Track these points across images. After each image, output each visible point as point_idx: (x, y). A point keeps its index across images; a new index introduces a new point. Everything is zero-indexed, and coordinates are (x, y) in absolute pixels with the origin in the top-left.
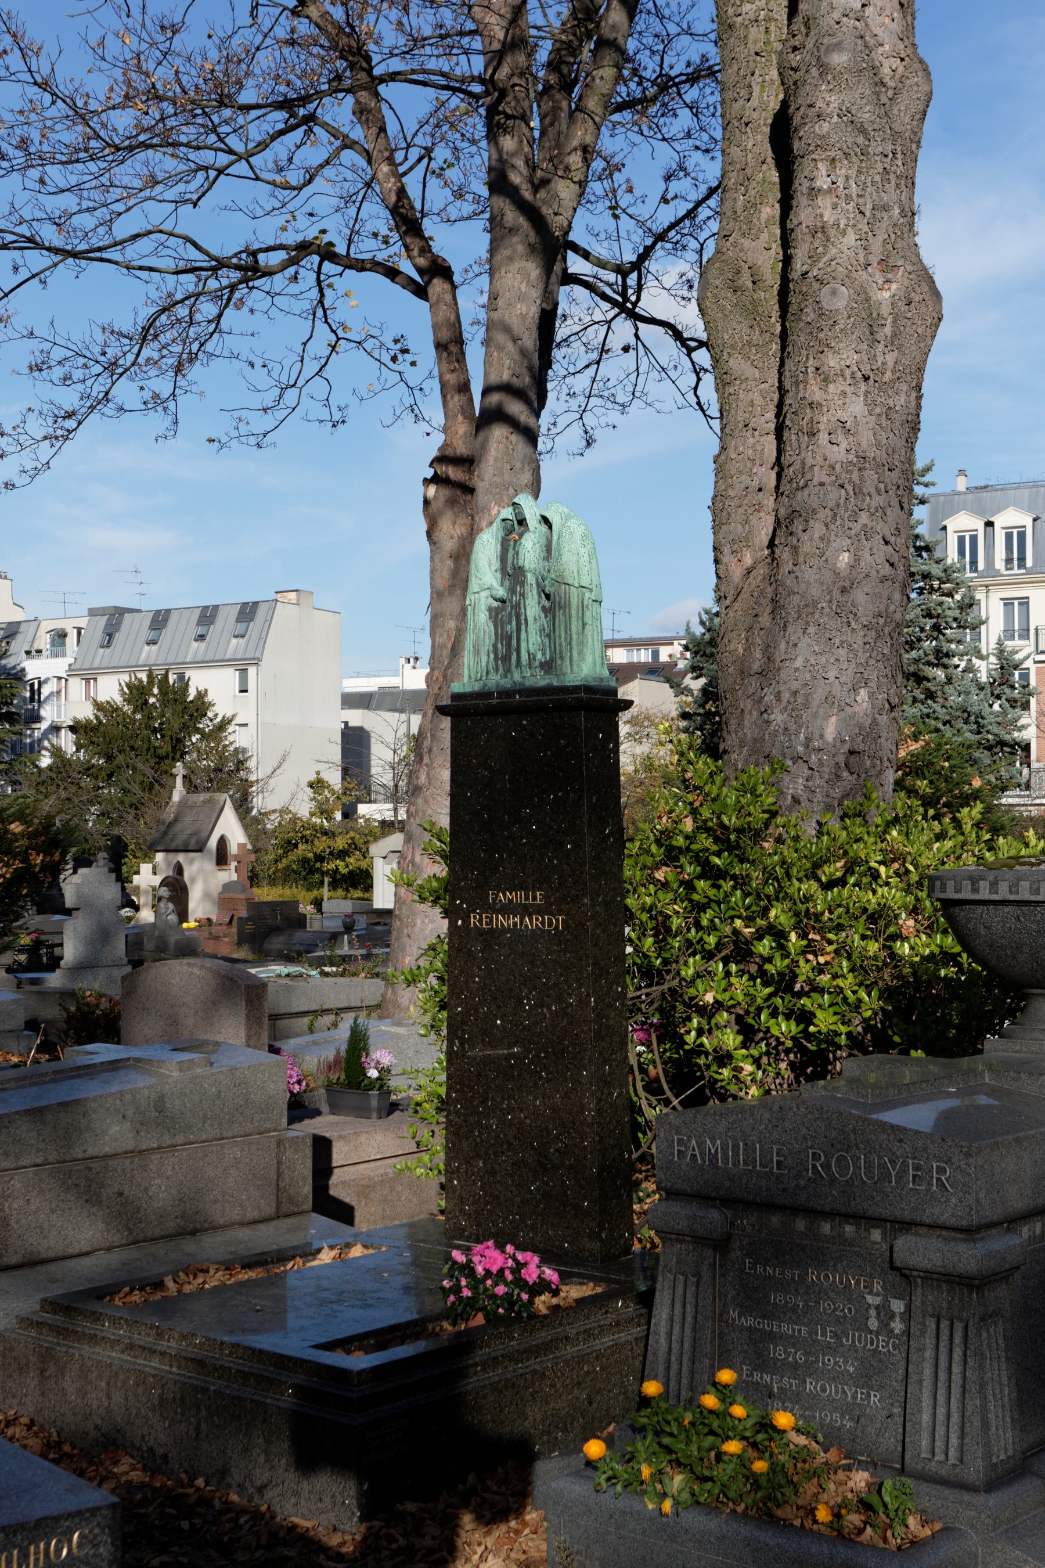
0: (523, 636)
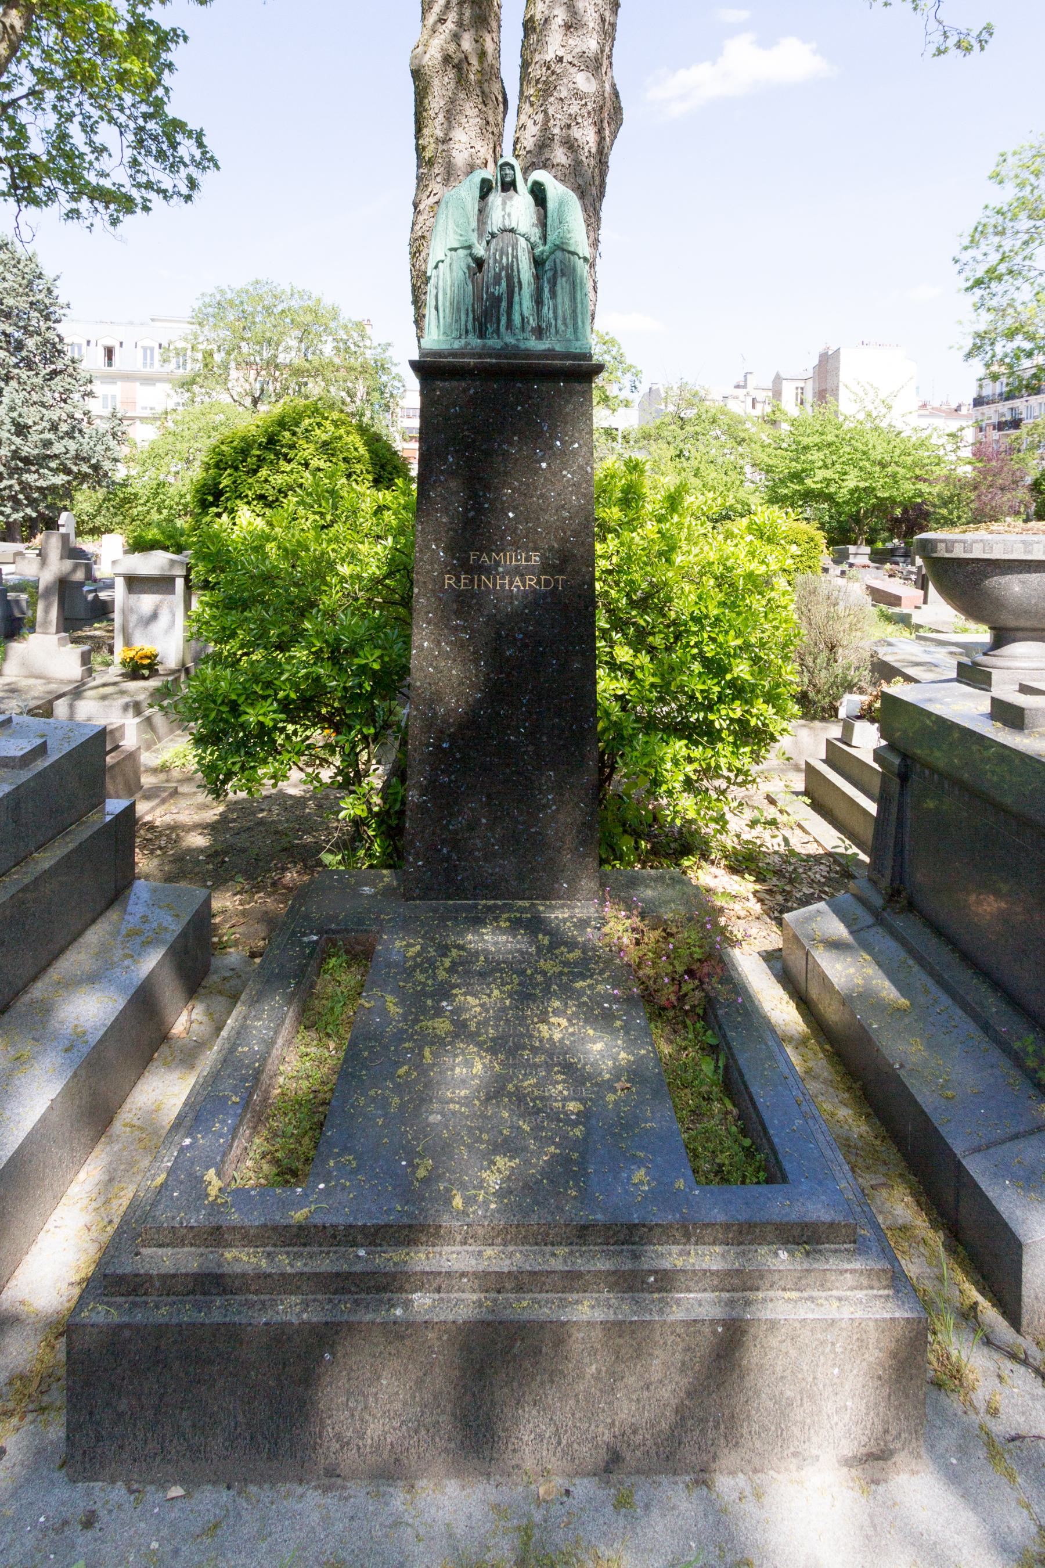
0: (516, 298)
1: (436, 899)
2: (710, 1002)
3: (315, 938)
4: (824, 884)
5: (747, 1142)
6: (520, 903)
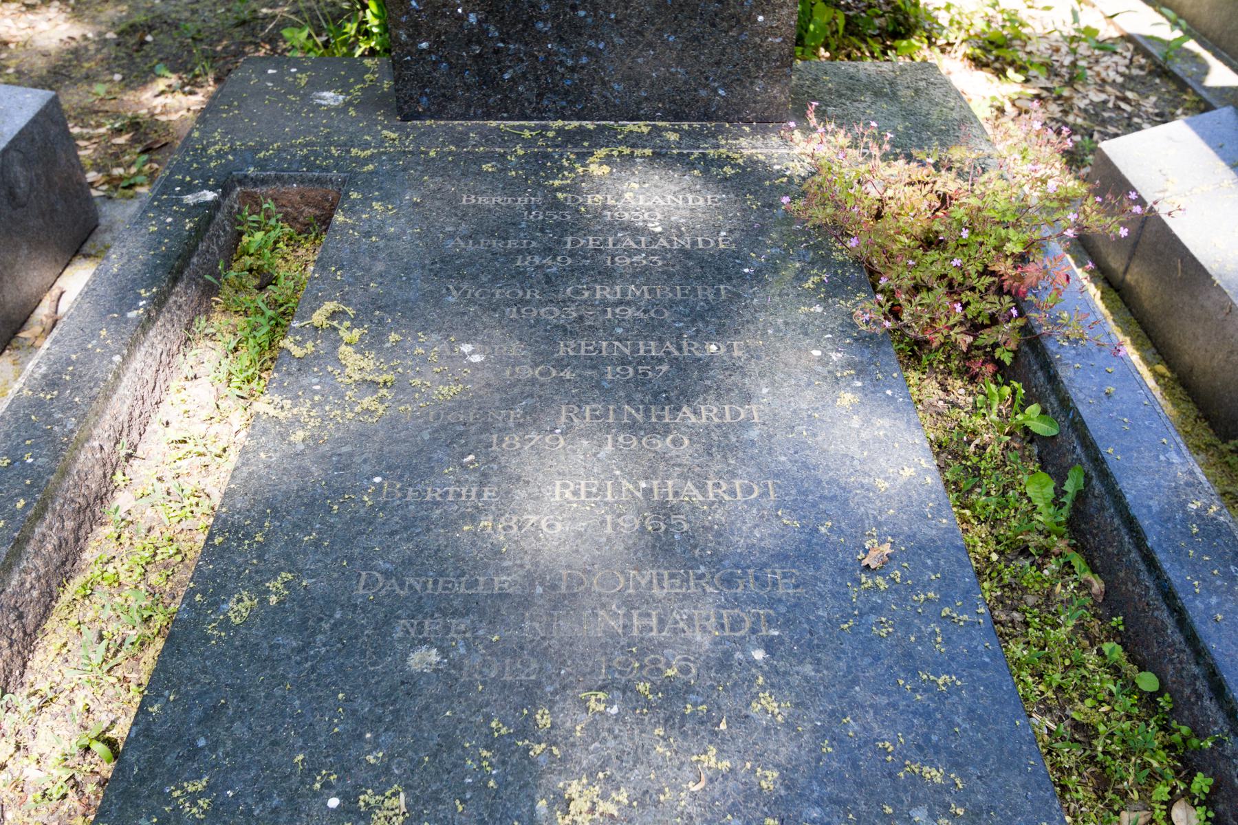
1: (465, 117)
2: (1032, 341)
3: (209, 196)
4: (1123, 87)
5: (1148, 682)
6: (631, 126)
